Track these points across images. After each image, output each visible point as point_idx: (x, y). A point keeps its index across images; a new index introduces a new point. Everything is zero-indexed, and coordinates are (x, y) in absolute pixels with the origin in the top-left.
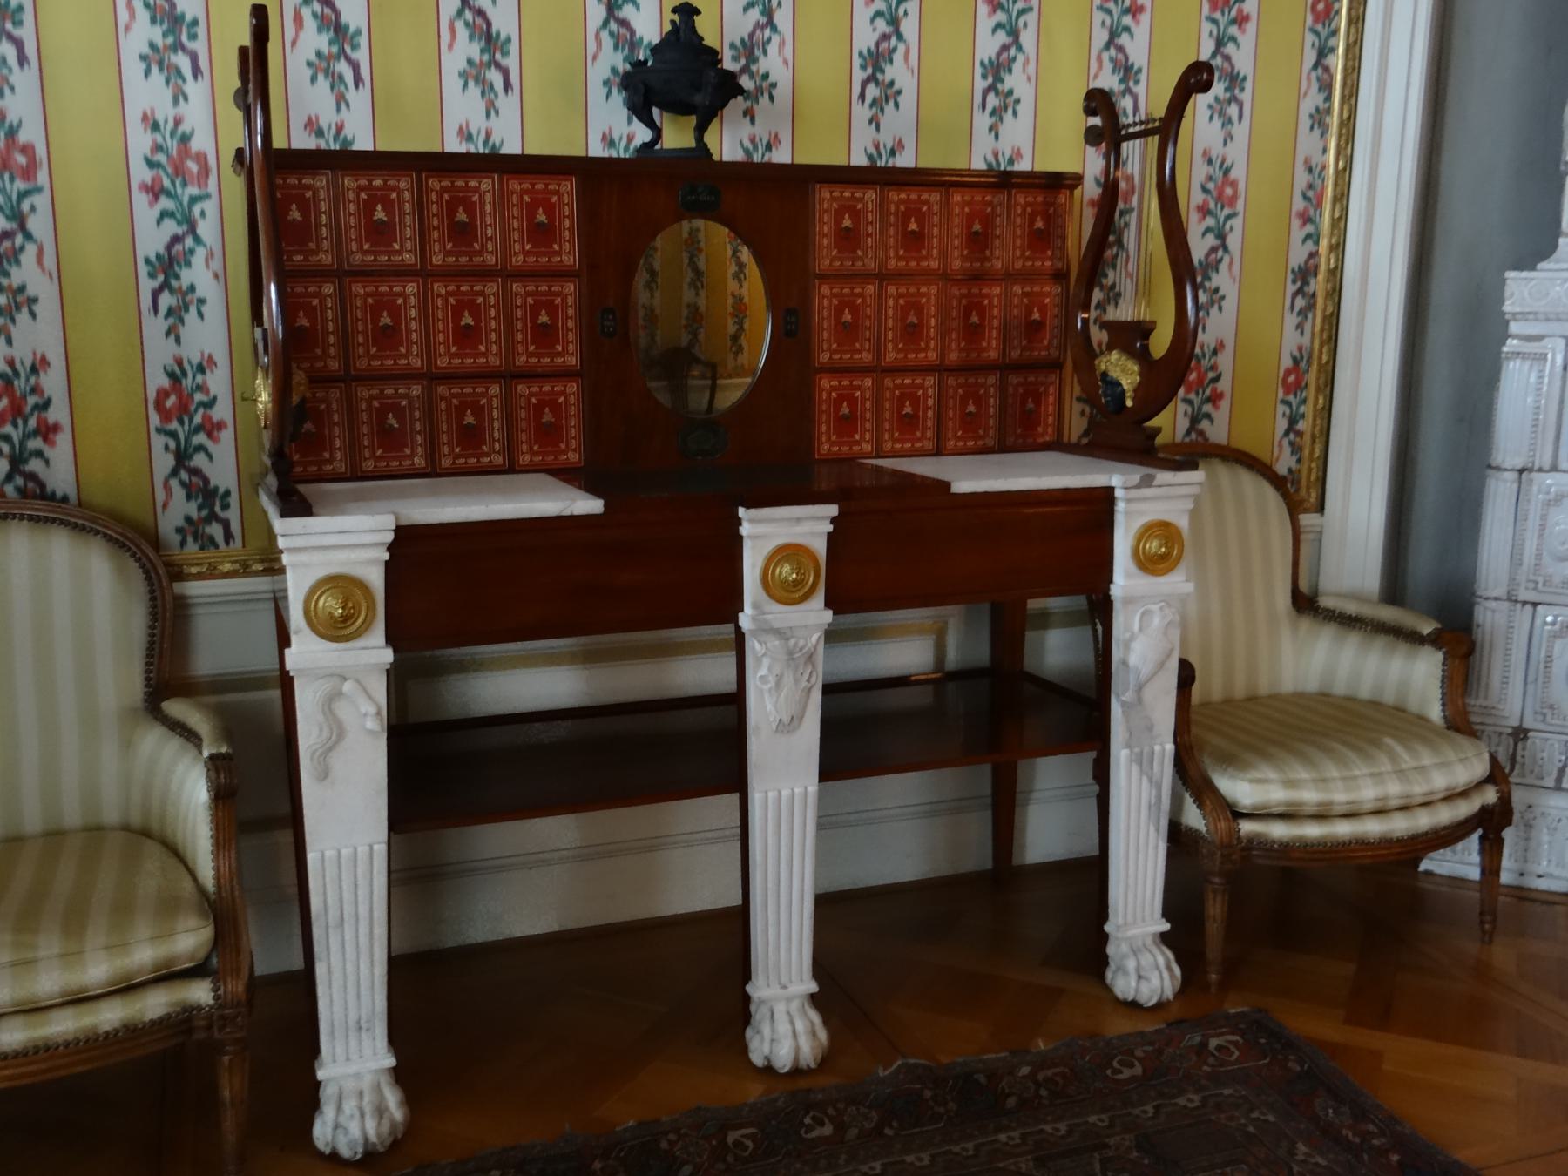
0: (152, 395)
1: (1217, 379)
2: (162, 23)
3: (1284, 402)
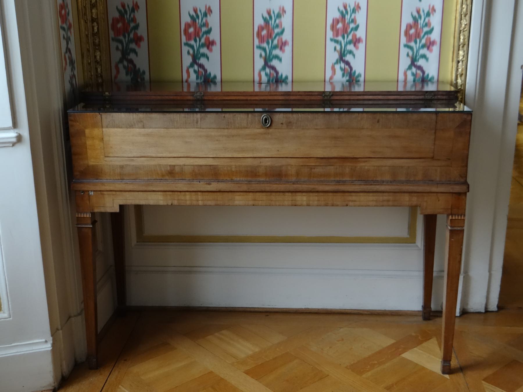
0: (330, 22)
1: (209, 31)
3: (259, 47)
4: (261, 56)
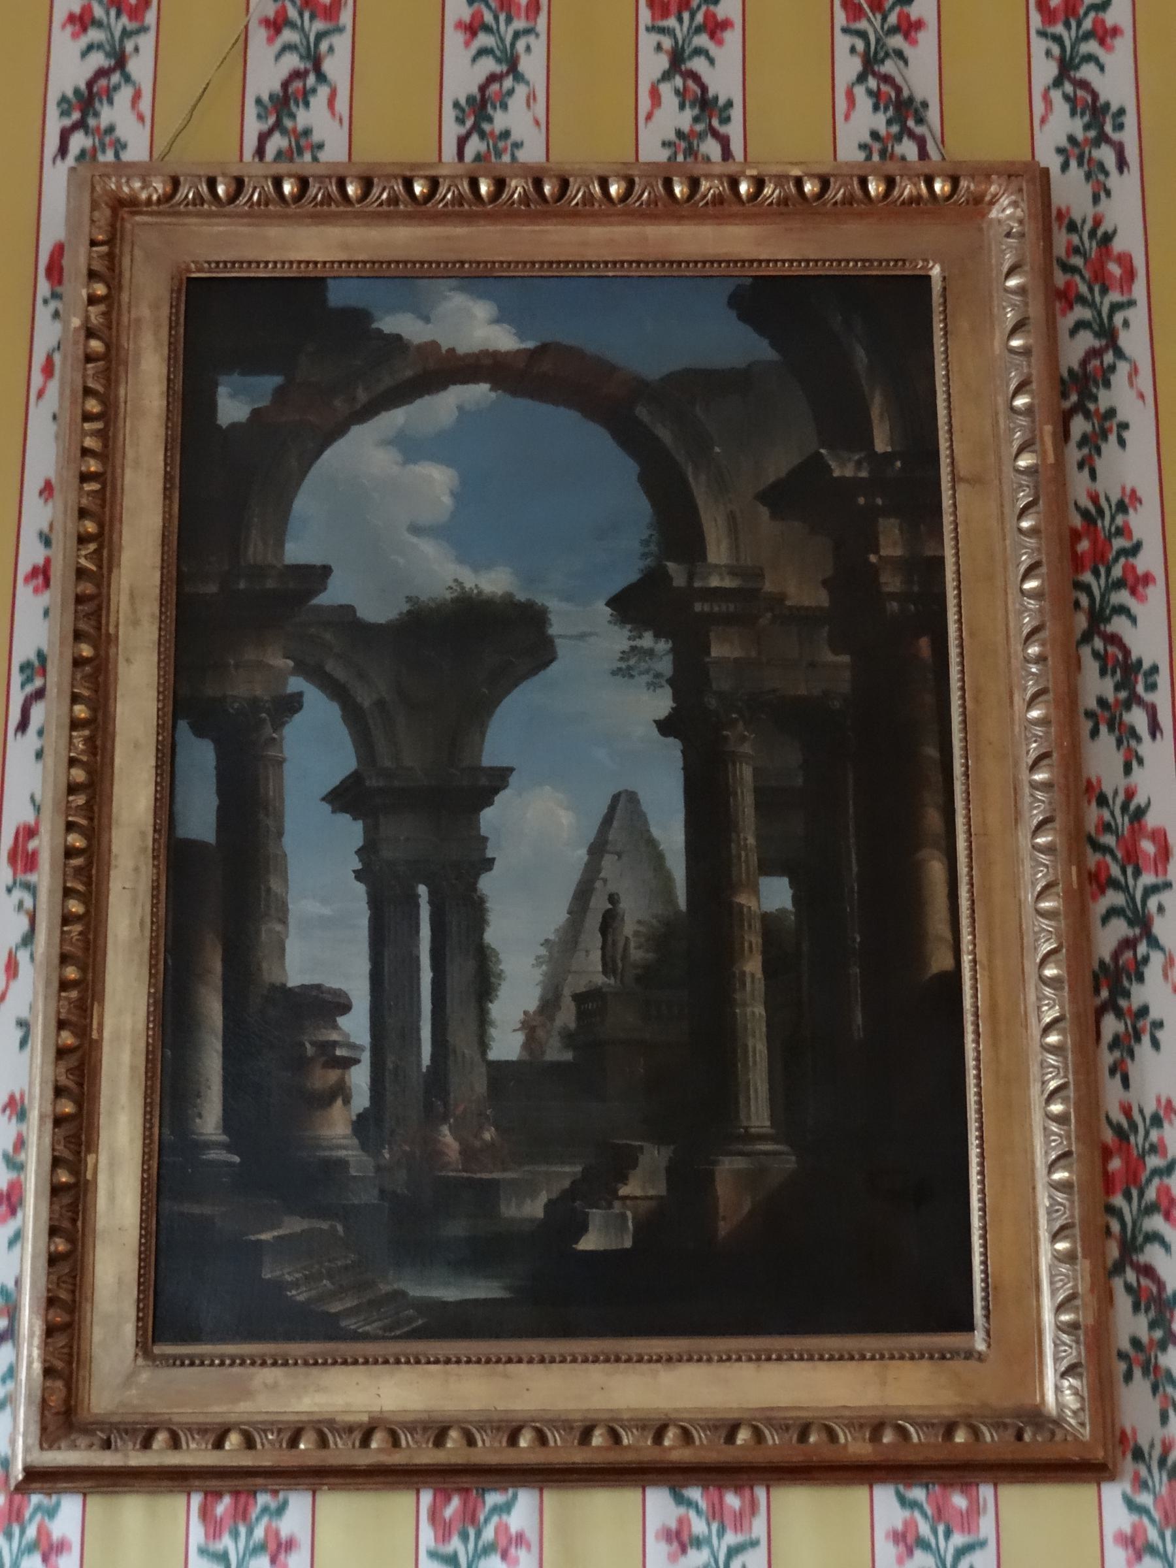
2: (1083, 114)
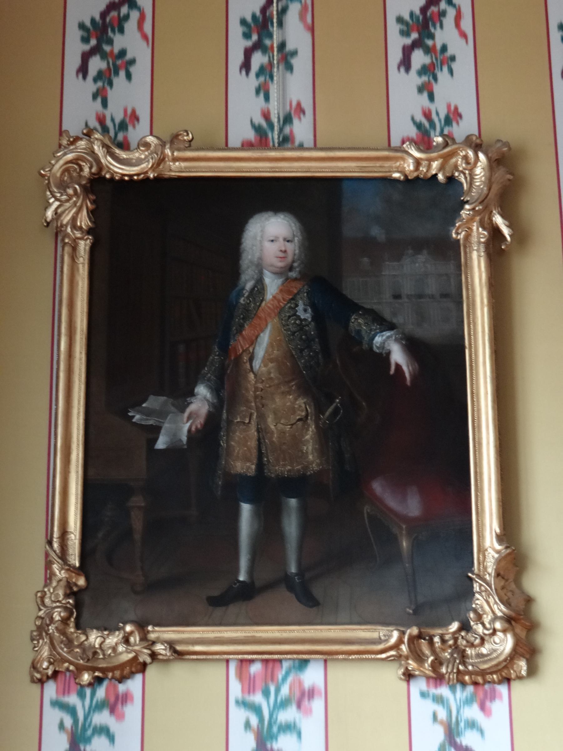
3: (244, 704)
4: (247, 725)
